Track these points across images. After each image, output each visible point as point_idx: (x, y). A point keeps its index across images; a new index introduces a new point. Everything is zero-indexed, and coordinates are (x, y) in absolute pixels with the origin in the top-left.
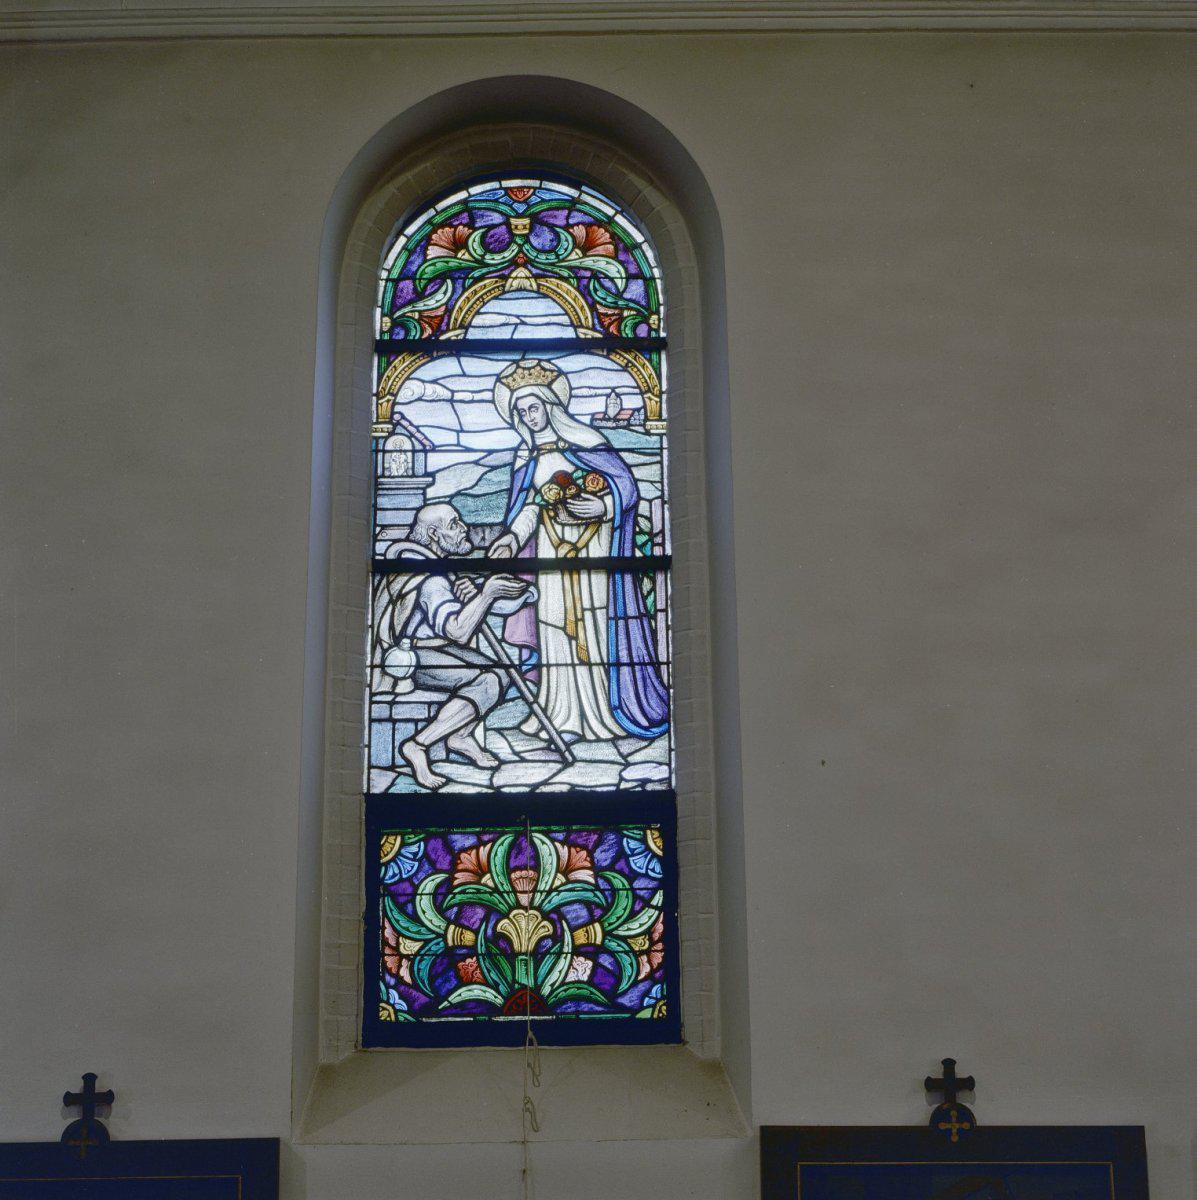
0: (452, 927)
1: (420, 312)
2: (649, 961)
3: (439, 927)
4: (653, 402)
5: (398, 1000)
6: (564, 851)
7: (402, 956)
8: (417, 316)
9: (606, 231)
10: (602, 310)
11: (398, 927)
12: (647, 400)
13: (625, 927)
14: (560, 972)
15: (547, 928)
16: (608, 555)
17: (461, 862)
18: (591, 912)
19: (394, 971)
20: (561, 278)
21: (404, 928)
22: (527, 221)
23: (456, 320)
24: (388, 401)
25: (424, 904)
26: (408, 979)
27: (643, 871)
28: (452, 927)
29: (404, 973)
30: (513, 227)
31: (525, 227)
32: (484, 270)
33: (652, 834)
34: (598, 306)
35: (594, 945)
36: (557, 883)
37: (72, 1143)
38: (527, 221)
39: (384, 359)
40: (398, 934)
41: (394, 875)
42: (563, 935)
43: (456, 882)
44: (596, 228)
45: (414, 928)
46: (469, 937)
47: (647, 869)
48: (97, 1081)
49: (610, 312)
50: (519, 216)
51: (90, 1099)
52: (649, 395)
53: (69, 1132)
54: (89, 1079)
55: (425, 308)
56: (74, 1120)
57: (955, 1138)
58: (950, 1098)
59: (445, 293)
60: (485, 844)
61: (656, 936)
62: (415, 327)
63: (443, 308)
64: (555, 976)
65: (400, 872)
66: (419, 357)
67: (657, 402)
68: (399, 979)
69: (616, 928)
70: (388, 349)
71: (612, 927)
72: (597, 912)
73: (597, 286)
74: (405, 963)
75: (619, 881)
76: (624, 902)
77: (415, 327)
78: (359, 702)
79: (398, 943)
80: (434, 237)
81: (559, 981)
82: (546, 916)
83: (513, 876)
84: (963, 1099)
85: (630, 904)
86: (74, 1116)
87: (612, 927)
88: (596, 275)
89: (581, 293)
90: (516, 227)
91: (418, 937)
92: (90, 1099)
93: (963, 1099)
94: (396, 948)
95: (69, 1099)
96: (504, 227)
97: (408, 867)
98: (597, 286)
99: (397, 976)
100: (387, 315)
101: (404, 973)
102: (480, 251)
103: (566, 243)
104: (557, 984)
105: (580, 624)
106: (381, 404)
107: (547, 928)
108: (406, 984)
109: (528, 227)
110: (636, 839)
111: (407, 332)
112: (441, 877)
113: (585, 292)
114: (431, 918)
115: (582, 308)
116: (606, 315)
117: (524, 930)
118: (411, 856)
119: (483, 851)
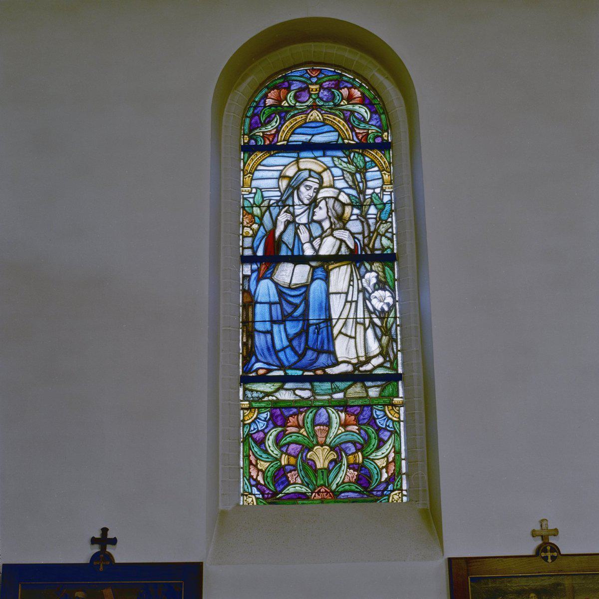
0: (284, 455)
1: (263, 132)
2: (387, 472)
3: (277, 455)
4: (387, 176)
5: (257, 493)
6: (343, 415)
7: (259, 470)
8: (261, 134)
9: (359, 91)
10: (358, 131)
11: (257, 455)
12: (384, 175)
13: (374, 454)
14: (341, 478)
15: (333, 456)
16: (333, 318)
17: (290, 422)
18: (356, 447)
19: (255, 477)
20: (336, 115)
21: (271, 434)
22: (317, 87)
23: (281, 137)
24: (249, 177)
25: (270, 442)
26: (262, 482)
27: (384, 426)
28: (284, 455)
29: (260, 478)
30: (311, 90)
31: (316, 90)
32: (296, 112)
33: (388, 408)
34: (356, 129)
35: (358, 464)
36: (340, 432)
37: (95, 563)
38: (317, 87)
39: (246, 155)
40: (257, 459)
41: (254, 429)
42: (342, 459)
43: (287, 432)
44: (353, 89)
45: (264, 456)
46: (292, 461)
47: (386, 426)
48: (108, 533)
49: (361, 132)
50: (312, 84)
51: (104, 540)
52: (385, 172)
53: (95, 557)
54: (105, 531)
55: (266, 130)
56: (98, 551)
57: (101, 568)
58: (103, 549)
59: (276, 122)
60: (302, 413)
61: (391, 459)
62: (261, 140)
63: (275, 130)
64: (338, 480)
65: (258, 428)
66: (264, 154)
67: (389, 175)
68: (258, 483)
69: (369, 455)
70: (249, 149)
71: (368, 454)
72: (360, 448)
73: (354, 119)
74: (260, 473)
75: (371, 430)
76: (374, 442)
77: (261, 140)
78: (238, 180)
79: (257, 464)
80: (269, 95)
81: (341, 481)
82: (332, 449)
83: (316, 428)
84: (110, 549)
85: (298, 485)
86: (96, 549)
87: (368, 454)
88: (352, 112)
89: (345, 121)
90: (312, 91)
91: (267, 460)
92: (104, 540)
93: (110, 549)
94: (256, 466)
95: (94, 541)
96: (272, 306)
97: (261, 425)
98: (354, 119)
99: (256, 480)
100: (246, 135)
101: (260, 478)
102: (293, 102)
103: (338, 97)
104: (340, 483)
105: (351, 287)
106: (246, 178)
107: (333, 456)
108: (261, 485)
109: (318, 90)
110: (380, 410)
111: (256, 141)
112: (280, 429)
113: (347, 121)
114: (274, 451)
115: (347, 130)
116: (360, 133)
117: (321, 457)
118: (263, 419)
119: (301, 417)
